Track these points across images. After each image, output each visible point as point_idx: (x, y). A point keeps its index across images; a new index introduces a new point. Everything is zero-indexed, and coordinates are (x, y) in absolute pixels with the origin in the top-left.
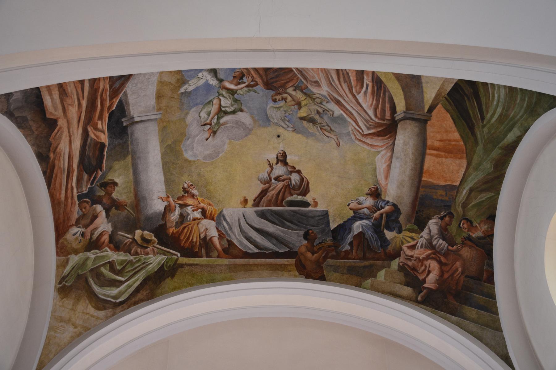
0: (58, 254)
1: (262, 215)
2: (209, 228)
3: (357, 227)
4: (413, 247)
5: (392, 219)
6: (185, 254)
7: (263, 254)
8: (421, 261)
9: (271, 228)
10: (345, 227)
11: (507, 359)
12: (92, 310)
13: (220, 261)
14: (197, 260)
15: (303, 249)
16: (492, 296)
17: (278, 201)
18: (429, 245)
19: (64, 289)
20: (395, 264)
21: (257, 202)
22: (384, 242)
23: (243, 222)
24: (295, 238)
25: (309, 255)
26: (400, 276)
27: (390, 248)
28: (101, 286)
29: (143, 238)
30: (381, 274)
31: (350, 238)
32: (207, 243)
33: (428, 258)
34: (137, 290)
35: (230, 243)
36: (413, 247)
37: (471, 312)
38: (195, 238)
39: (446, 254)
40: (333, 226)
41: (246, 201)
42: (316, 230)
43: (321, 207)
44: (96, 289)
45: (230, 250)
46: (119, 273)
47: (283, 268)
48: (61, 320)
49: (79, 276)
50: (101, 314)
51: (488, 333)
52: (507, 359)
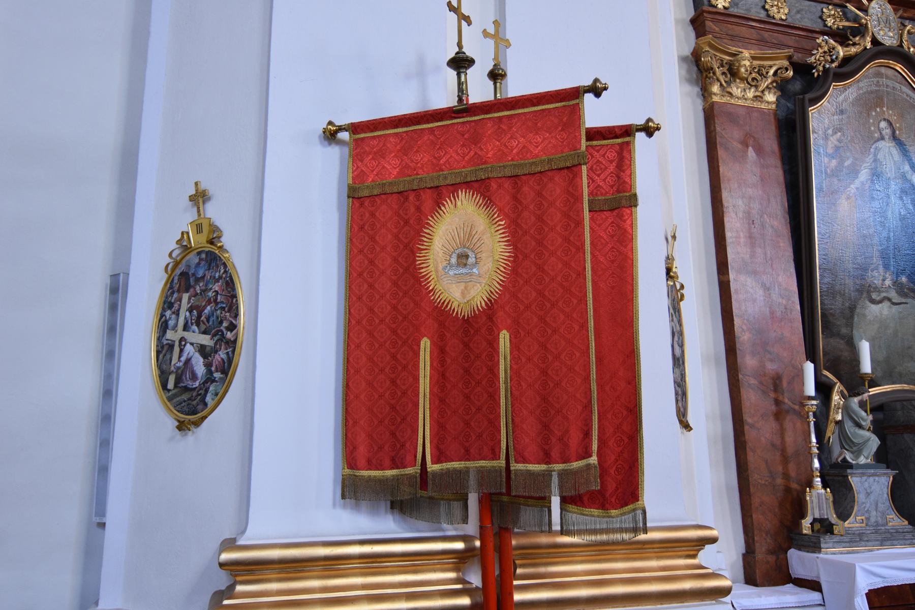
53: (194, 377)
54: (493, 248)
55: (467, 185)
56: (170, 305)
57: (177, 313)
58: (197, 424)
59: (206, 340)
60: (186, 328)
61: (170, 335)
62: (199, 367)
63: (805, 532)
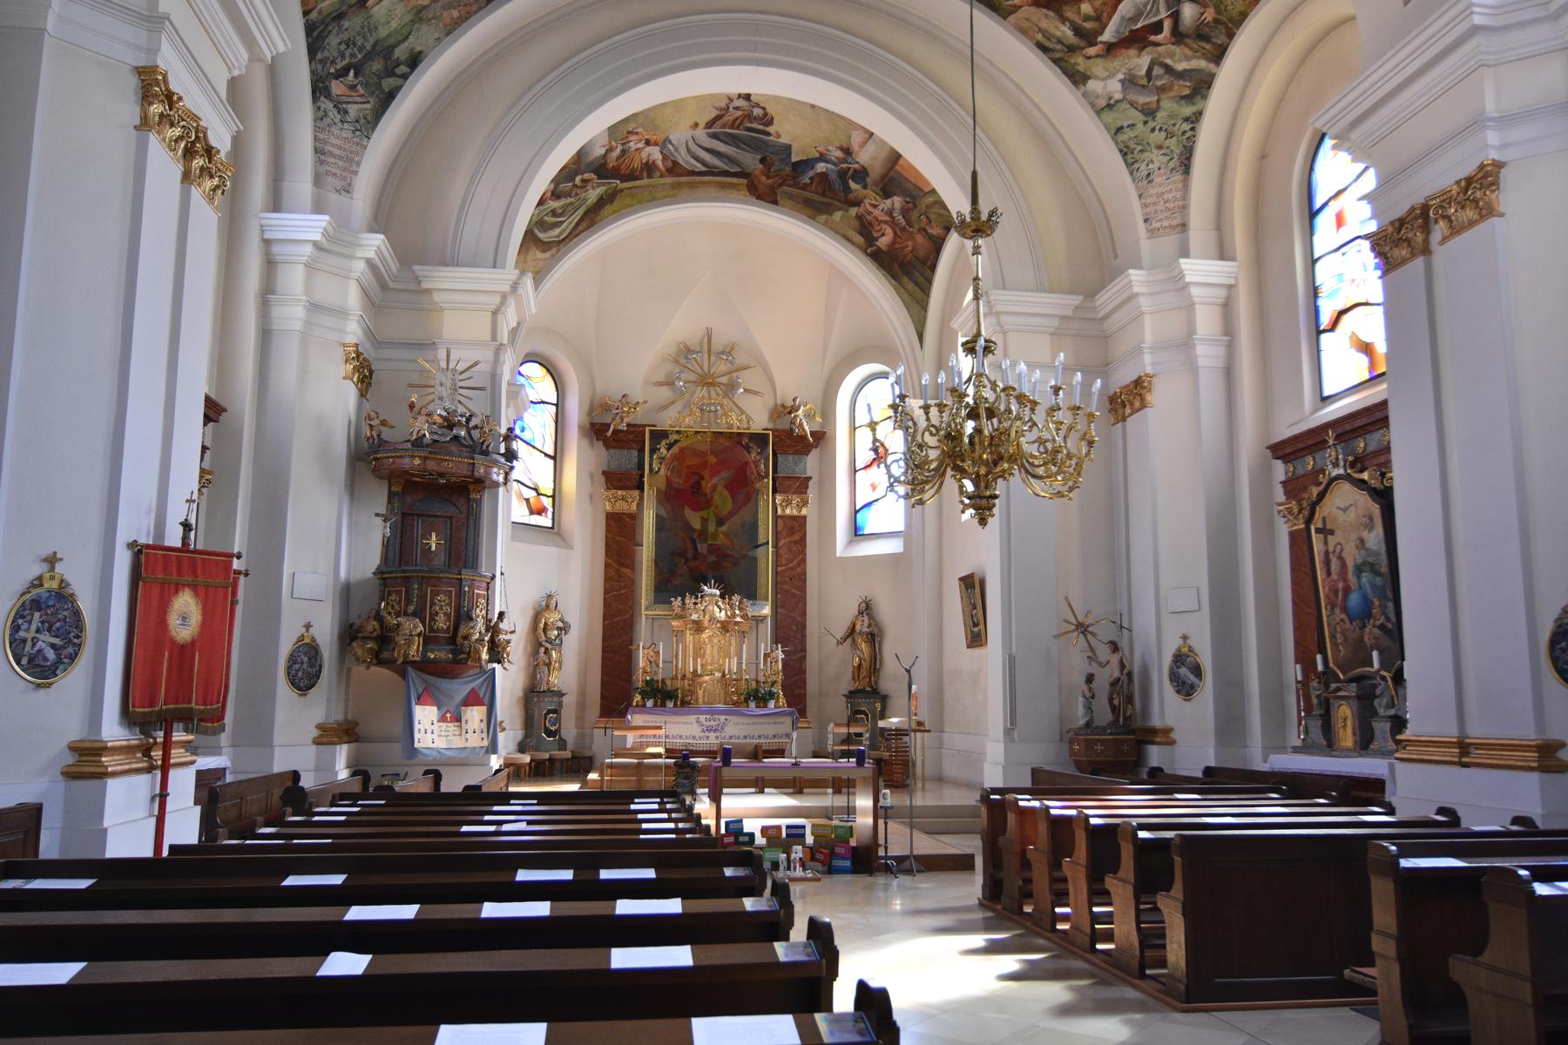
1: (714, 136)
2: (655, 154)
3: (821, 167)
4: (875, 206)
5: (861, 175)
6: (624, 179)
7: (711, 171)
8: (880, 222)
9: (722, 148)
10: (807, 164)
11: (921, 336)
12: (540, 255)
13: (662, 180)
14: (637, 183)
15: (758, 172)
16: (930, 282)
17: (734, 124)
18: (890, 213)
20: (853, 211)
21: (709, 125)
22: (847, 190)
23: (691, 144)
24: (751, 161)
25: (763, 178)
26: (856, 224)
27: (851, 196)
28: (545, 231)
29: (583, 181)
30: (838, 215)
31: (811, 173)
32: (649, 168)
33: (886, 222)
34: (578, 224)
35: (675, 163)
36: (875, 206)
37: (910, 286)
38: (636, 164)
39: (903, 229)
40: (794, 159)
41: (696, 125)
42: (774, 158)
43: (784, 140)
44: (541, 235)
45: (674, 169)
46: (561, 215)
47: (734, 186)
50: (548, 254)
51: (916, 308)
52: (921, 336)
53: (46, 659)
54: (196, 617)
55: (189, 586)
56: (23, 617)
57: (30, 623)
58: (49, 685)
59: (56, 641)
60: (38, 631)
61: (22, 634)
62: (51, 655)
63: (901, 550)
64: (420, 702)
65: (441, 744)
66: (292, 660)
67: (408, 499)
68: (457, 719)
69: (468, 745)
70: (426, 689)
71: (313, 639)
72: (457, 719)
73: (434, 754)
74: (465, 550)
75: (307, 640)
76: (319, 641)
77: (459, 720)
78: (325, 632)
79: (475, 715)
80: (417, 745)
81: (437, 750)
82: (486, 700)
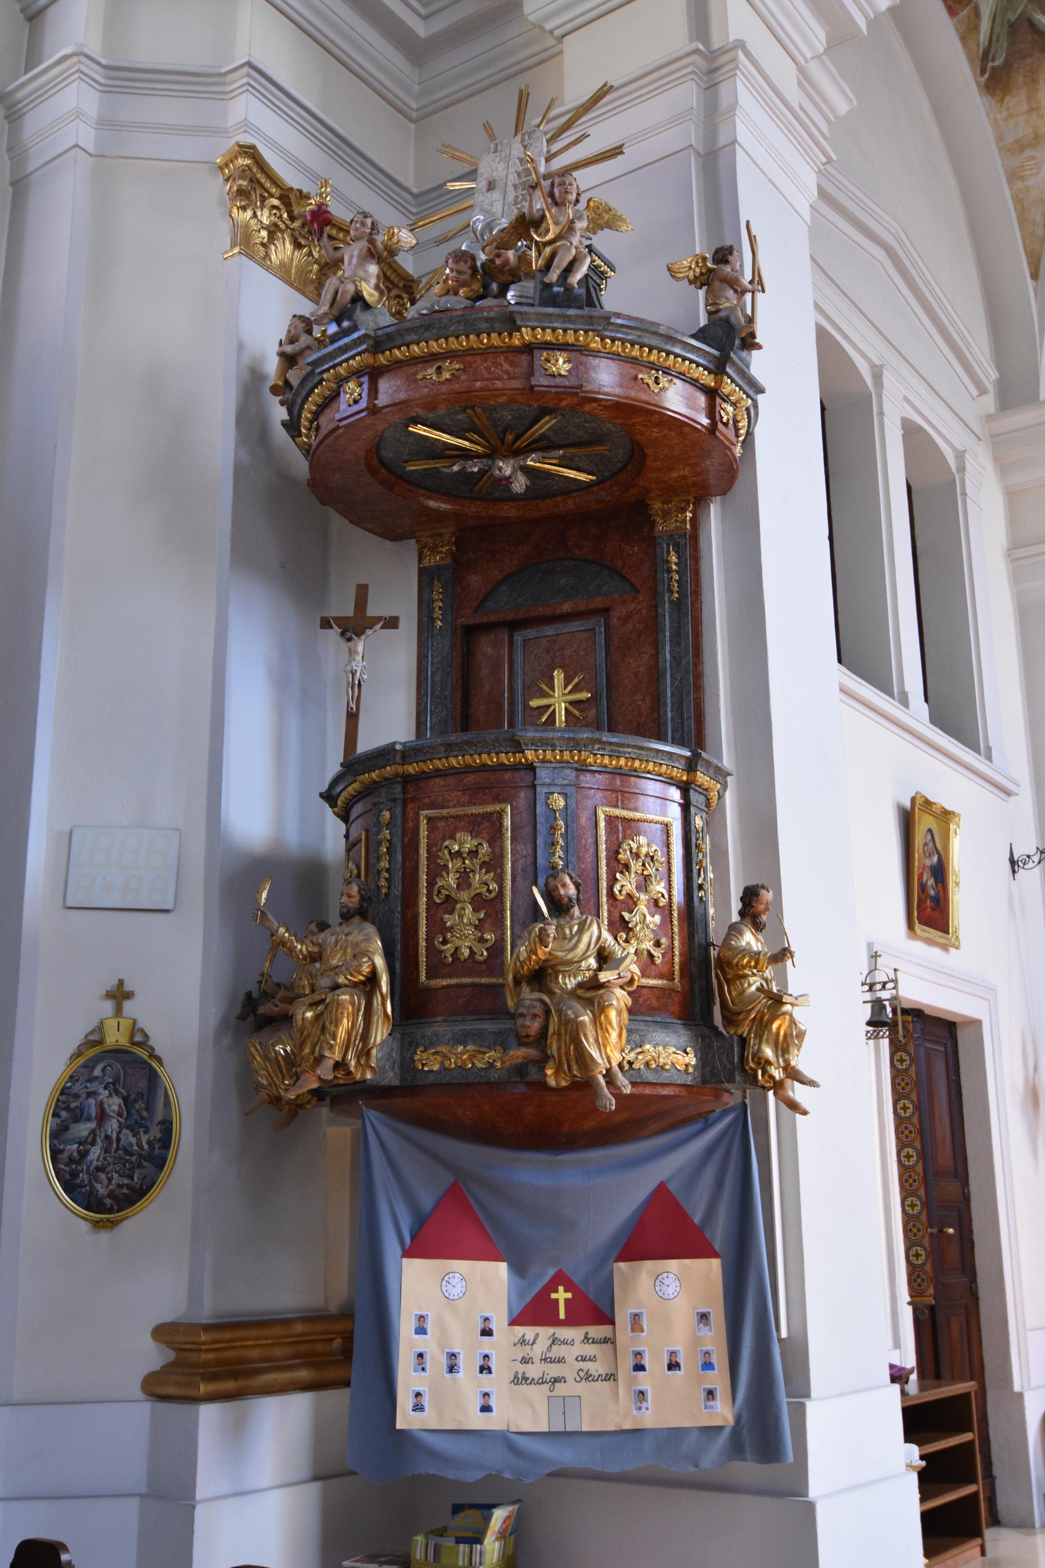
0: (952, 12)
19: (996, 80)
48: (1021, 146)
49: (1013, 28)
64: (423, 1245)
65: (522, 1413)
66: (67, 1107)
67: (475, 580)
68: (595, 1311)
69: (650, 1418)
70: (455, 1196)
71: (139, 1038)
72: (595, 1311)
73: (495, 1458)
74: (661, 687)
75: (116, 1037)
76: (159, 1042)
77: (604, 1316)
78: (180, 1011)
79: (671, 1296)
80: (405, 1419)
81: (505, 1439)
82: (719, 1234)
